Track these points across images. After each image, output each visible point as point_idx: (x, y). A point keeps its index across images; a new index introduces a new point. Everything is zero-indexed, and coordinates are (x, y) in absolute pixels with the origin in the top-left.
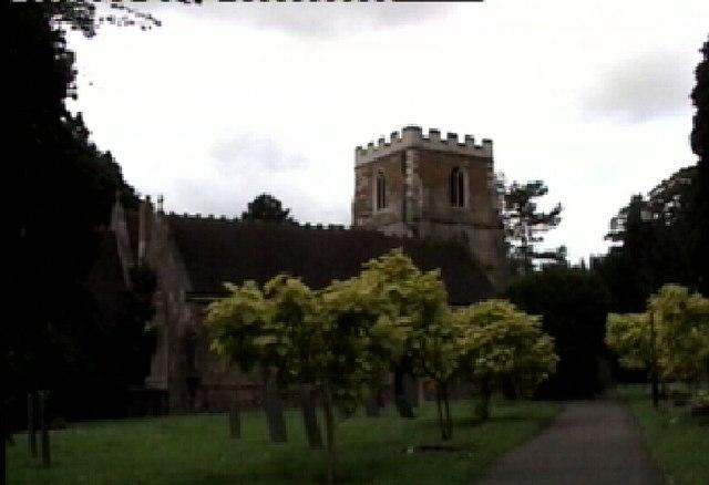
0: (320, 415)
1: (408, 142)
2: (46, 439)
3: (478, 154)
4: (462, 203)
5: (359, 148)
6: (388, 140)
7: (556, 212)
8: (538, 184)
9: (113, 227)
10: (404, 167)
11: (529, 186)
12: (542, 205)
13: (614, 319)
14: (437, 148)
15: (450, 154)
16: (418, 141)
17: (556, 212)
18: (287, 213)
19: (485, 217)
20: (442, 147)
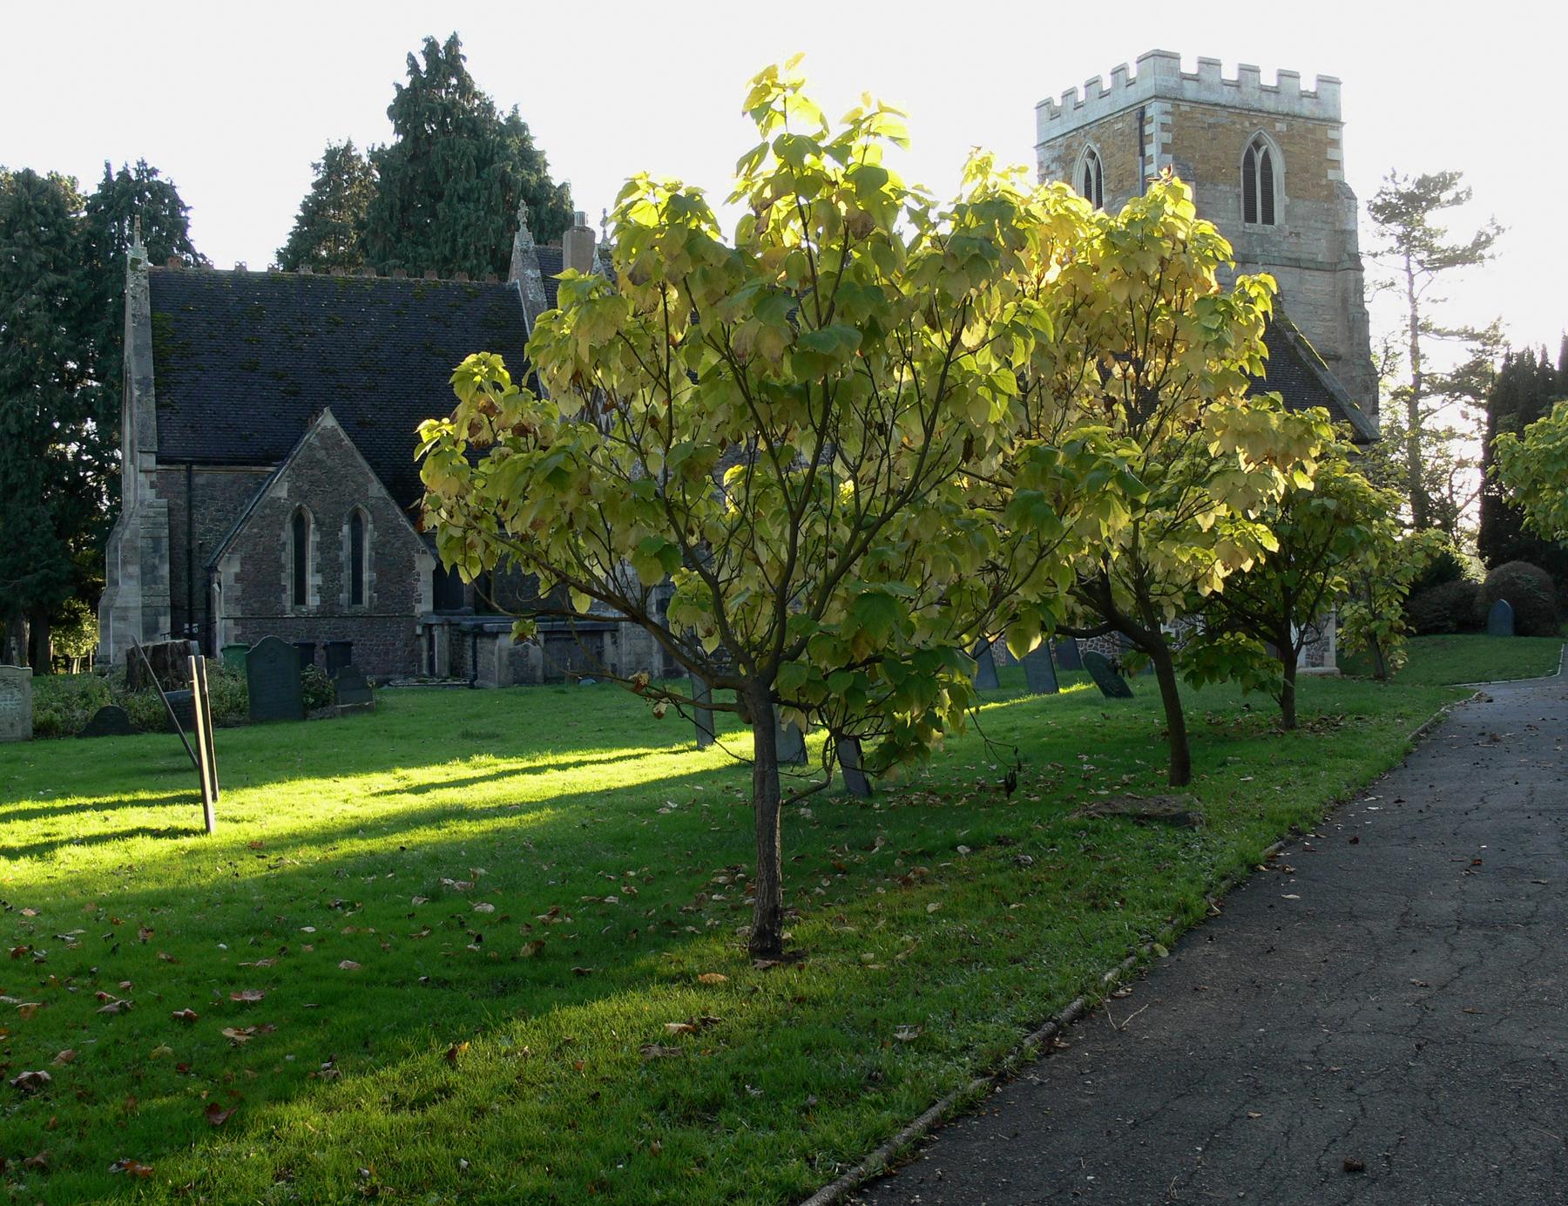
0: (763, 627)
1: (1147, 87)
2: (475, 644)
3: (1307, 108)
4: (1269, 218)
5: (1047, 103)
6: (1107, 84)
7: (1482, 242)
8: (1445, 182)
9: (514, 279)
10: (1142, 140)
11: (1424, 182)
12: (1449, 225)
13: (427, 430)
14: (1213, 98)
15: (1246, 111)
16: (1172, 82)
17: (1482, 242)
18: (297, 217)
19: (1320, 250)
20: (1227, 96)
